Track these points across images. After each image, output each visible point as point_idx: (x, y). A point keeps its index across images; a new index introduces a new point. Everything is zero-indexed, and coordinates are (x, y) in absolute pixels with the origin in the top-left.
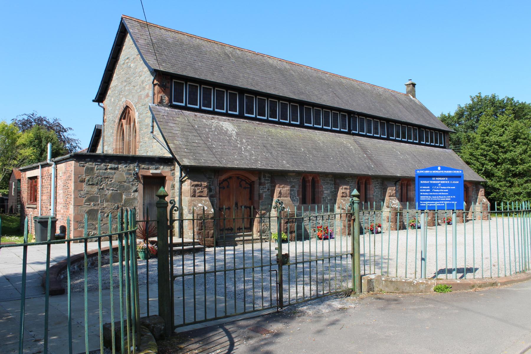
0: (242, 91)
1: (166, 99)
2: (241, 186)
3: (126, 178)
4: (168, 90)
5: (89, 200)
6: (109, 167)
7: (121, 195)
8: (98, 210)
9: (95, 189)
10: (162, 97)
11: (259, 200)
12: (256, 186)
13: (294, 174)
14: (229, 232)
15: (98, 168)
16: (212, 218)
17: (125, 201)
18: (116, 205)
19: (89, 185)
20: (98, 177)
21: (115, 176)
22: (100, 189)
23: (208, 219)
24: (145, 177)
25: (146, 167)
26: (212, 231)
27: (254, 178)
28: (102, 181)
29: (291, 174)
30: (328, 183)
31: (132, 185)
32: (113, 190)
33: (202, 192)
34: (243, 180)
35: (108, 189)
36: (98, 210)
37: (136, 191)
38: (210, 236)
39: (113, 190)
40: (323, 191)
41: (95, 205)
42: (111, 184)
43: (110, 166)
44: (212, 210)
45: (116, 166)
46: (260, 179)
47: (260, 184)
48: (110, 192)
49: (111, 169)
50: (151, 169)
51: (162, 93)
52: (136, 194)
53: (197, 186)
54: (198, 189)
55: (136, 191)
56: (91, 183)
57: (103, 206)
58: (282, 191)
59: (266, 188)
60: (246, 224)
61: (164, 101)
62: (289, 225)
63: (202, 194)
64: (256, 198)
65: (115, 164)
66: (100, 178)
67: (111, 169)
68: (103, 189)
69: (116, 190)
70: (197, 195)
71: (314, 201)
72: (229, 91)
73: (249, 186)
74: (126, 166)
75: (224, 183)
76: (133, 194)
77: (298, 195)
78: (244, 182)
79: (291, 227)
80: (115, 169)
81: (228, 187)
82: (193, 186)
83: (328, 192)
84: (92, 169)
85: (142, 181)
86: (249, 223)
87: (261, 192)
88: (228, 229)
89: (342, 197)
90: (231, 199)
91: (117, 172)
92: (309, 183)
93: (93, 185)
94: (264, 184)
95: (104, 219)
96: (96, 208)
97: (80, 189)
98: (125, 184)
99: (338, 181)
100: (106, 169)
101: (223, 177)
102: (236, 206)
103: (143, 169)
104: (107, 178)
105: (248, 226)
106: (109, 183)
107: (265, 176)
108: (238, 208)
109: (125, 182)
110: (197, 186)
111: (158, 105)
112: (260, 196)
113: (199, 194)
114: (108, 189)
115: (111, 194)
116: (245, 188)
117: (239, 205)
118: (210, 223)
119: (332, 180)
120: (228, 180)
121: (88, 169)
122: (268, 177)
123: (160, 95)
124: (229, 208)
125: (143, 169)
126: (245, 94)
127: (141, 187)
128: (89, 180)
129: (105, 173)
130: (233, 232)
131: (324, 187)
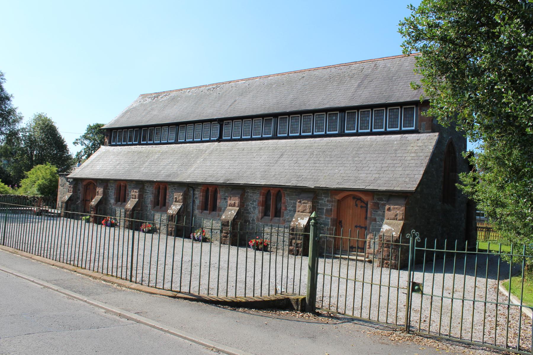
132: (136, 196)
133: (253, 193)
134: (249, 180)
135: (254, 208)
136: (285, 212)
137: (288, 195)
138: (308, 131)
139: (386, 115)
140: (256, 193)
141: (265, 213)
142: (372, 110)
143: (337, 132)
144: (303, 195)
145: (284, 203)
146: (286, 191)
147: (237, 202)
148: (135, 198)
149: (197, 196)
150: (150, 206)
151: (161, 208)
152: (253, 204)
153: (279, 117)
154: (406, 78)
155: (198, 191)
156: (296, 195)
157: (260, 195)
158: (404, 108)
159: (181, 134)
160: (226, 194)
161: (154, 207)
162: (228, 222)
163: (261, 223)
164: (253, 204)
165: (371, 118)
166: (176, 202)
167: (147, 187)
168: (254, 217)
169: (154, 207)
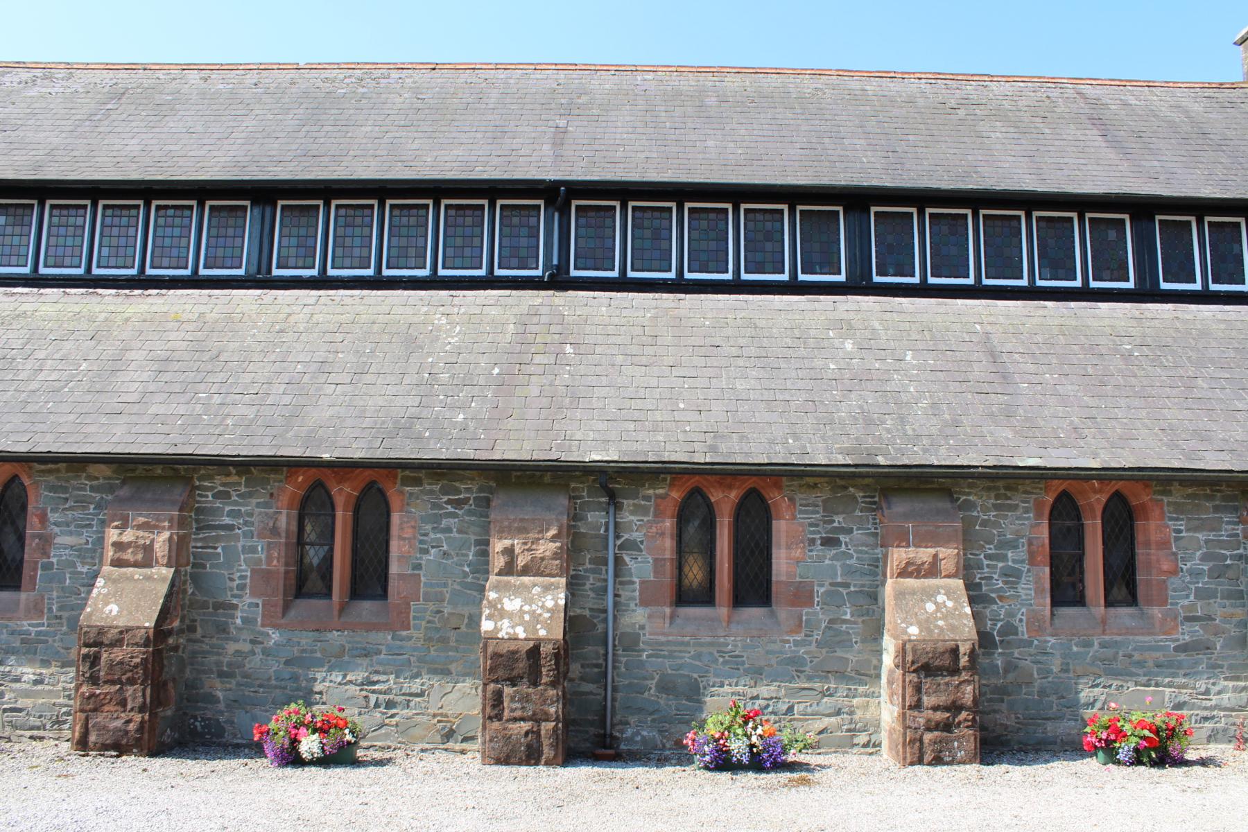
0: (857, 200)
30: (82, 503)
71: (754, 586)
119: (111, 489)
131: (53, 517)
132: (148, 549)
133: (997, 507)
134: (256, 441)
135: (1011, 575)
136: (1174, 582)
137: (1179, 508)
138: (768, 266)
139: (491, 227)
140: (1014, 508)
141: (1066, 591)
142: (201, 205)
143: (241, 272)
144: (900, 506)
145: (1164, 545)
146: (1168, 493)
147: (161, 541)
148: (147, 563)
149: (637, 536)
150: (247, 605)
151: (343, 608)
152: (1003, 558)
153: (280, 203)
154: (925, 132)
155: (639, 510)
156: (1217, 509)
157: (1039, 515)
158: (212, 207)
159: (763, 252)
160: (839, 520)
161: (286, 608)
162: (955, 652)
163: (1052, 640)
164: (1003, 558)
165: (380, 226)
166: (509, 569)
167: (224, 496)
168: (1011, 614)
169: (286, 608)
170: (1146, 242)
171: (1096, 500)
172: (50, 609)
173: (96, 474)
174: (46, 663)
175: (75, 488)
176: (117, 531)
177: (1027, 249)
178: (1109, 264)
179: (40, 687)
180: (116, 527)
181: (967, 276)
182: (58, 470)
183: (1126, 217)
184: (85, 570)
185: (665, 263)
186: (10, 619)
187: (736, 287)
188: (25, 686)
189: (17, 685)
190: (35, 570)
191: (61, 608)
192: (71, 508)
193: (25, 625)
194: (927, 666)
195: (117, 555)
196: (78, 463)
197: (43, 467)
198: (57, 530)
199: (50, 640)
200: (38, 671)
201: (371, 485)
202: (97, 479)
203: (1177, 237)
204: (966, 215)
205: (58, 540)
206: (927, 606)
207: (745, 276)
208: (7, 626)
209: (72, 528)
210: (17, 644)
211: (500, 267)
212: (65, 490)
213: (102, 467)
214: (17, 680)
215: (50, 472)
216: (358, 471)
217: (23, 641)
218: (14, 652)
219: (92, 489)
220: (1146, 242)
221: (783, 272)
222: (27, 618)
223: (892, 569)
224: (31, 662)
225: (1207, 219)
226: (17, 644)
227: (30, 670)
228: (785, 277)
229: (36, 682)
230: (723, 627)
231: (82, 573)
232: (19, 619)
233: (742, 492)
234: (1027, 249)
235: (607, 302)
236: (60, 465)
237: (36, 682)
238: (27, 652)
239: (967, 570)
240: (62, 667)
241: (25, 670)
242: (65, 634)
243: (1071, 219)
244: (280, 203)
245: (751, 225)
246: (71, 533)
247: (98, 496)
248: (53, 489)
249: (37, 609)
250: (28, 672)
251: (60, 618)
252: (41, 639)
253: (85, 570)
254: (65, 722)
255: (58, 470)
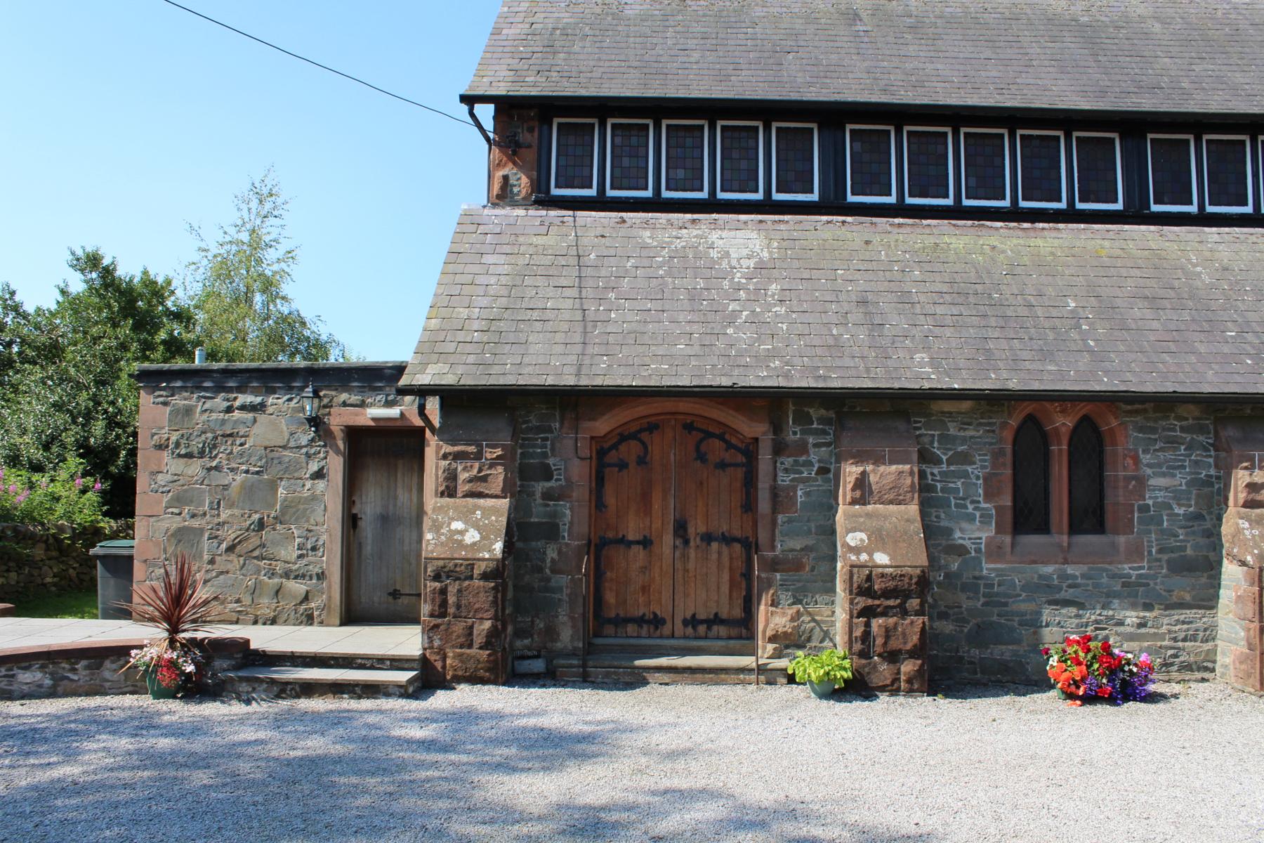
0: (833, 115)
1: (522, 183)
2: (702, 457)
3: (286, 435)
4: (530, 155)
5: (179, 500)
6: (237, 403)
7: (273, 486)
8: (201, 531)
9: (195, 468)
10: (506, 178)
11: (775, 511)
12: (765, 457)
13: (966, 405)
14: (644, 631)
15: (207, 406)
16: (485, 576)
17: (285, 509)
18: (256, 517)
19: (180, 456)
20: (204, 432)
21: (256, 430)
22: (209, 469)
23: (471, 578)
24: (355, 434)
25: (355, 398)
26: (487, 624)
27: (752, 428)
28: (215, 446)
29: (948, 406)
30: (1173, 443)
31: (308, 456)
32: (247, 472)
33: (484, 479)
34: (709, 435)
35: (232, 470)
36: (202, 531)
37: (319, 475)
38: (478, 639)
39: (247, 472)
40: (1141, 481)
41: (193, 516)
42: (241, 455)
43: (243, 399)
44: (498, 546)
45: (259, 399)
46: (777, 428)
47: (779, 449)
48: (240, 478)
49: (243, 408)
50: (371, 405)
51: (510, 165)
52: (321, 485)
53: (458, 456)
54: (465, 469)
55: (319, 475)
56: (183, 452)
57: (216, 520)
58: (873, 478)
59: (811, 464)
60: (720, 600)
61: (515, 190)
62: (877, 624)
63: (481, 488)
64: (764, 505)
65: (255, 392)
66: (210, 435)
67: (243, 408)
68: (217, 468)
69: (257, 473)
70: (462, 488)
71: (1091, 516)
72: (1019, 132)
73: (741, 459)
74: (290, 400)
75: (623, 447)
76: (309, 484)
77: (988, 496)
78: (717, 443)
79: (888, 633)
80: (253, 408)
81: (642, 461)
82: (445, 457)
83: (1179, 480)
84: (188, 411)
85: (341, 444)
86: (740, 601)
87: (784, 479)
88: (640, 621)
89: (1250, 504)
90: (656, 506)
91: (262, 418)
92: (1059, 444)
93: (189, 456)
94: (802, 448)
95: (218, 559)
96: (195, 523)
97: (155, 468)
98: (286, 453)
99: (1230, 432)
100: (229, 410)
101: (603, 425)
102: (676, 534)
103: (345, 404)
104: (231, 435)
105: (738, 613)
106: (236, 449)
107: (804, 419)
108: (687, 543)
109: (284, 447)
110: (458, 456)
111: (495, 205)
112: (779, 499)
113: (467, 487)
114: (232, 470)
115: (243, 486)
116: (722, 465)
117: (691, 531)
118: (480, 593)
119: (1202, 430)
120: (645, 436)
121: (176, 412)
122: (822, 420)
123: (500, 173)
124: (646, 543)
125: (345, 404)
126: (1150, 136)
127: (336, 465)
128: (177, 445)
129: (223, 422)
130: (666, 630)
131: (1146, 458)
141: (1027, 516)
170: (1142, 159)
171: (1064, 423)
172: (1150, 552)
173: (1185, 415)
174: (1148, 607)
175: (1164, 429)
176: (1247, 473)
177: (1011, 167)
178: (1097, 185)
179: (1143, 630)
180: (1246, 468)
181: (1116, 201)
182: (1145, 411)
183: (815, 126)
184: (1181, 512)
185: (697, 183)
186: (1110, 563)
187: (1014, 215)
188: (1129, 630)
189: (1121, 629)
190: (1132, 512)
191: (1160, 551)
192: (1161, 449)
193: (1126, 568)
194: (873, 595)
195: (1251, 496)
196: (1163, 405)
197: (1129, 407)
198: (1149, 471)
199: (1151, 583)
200: (1142, 614)
201: (1031, 420)
202: (1187, 419)
203: (874, 147)
204: (1058, 138)
205: (1152, 482)
206: (873, 529)
207: (721, 195)
208: (1106, 570)
209: (1164, 469)
210: (1118, 588)
211: (557, 186)
212: (1153, 430)
213: (1192, 407)
214: (1121, 623)
215: (1137, 412)
216: (1026, 404)
217: (1124, 585)
218: (1117, 595)
219: (1183, 429)
220: (1142, 159)
221: (812, 192)
222: (1128, 561)
223: (844, 496)
224: (1134, 606)
225: (1019, 132)
226: (1118, 588)
227: (1134, 614)
228: (704, 195)
229: (1141, 625)
230: (1048, 559)
231: (1178, 515)
232: (1120, 563)
233: (1022, 416)
234: (1011, 167)
235: (557, 221)
236: (1147, 405)
237: (1141, 625)
238: (1129, 595)
239: (925, 492)
240: (1166, 609)
241: (1128, 613)
242: (1165, 576)
243: (945, 134)
244: (556, 121)
245: (618, 140)
246: (1164, 475)
247: (1188, 437)
248: (1141, 430)
249: (1136, 553)
250: (1131, 617)
251: (1159, 560)
252: (1142, 582)
253: (1181, 512)
254: (1172, 664)
255: (1145, 411)
